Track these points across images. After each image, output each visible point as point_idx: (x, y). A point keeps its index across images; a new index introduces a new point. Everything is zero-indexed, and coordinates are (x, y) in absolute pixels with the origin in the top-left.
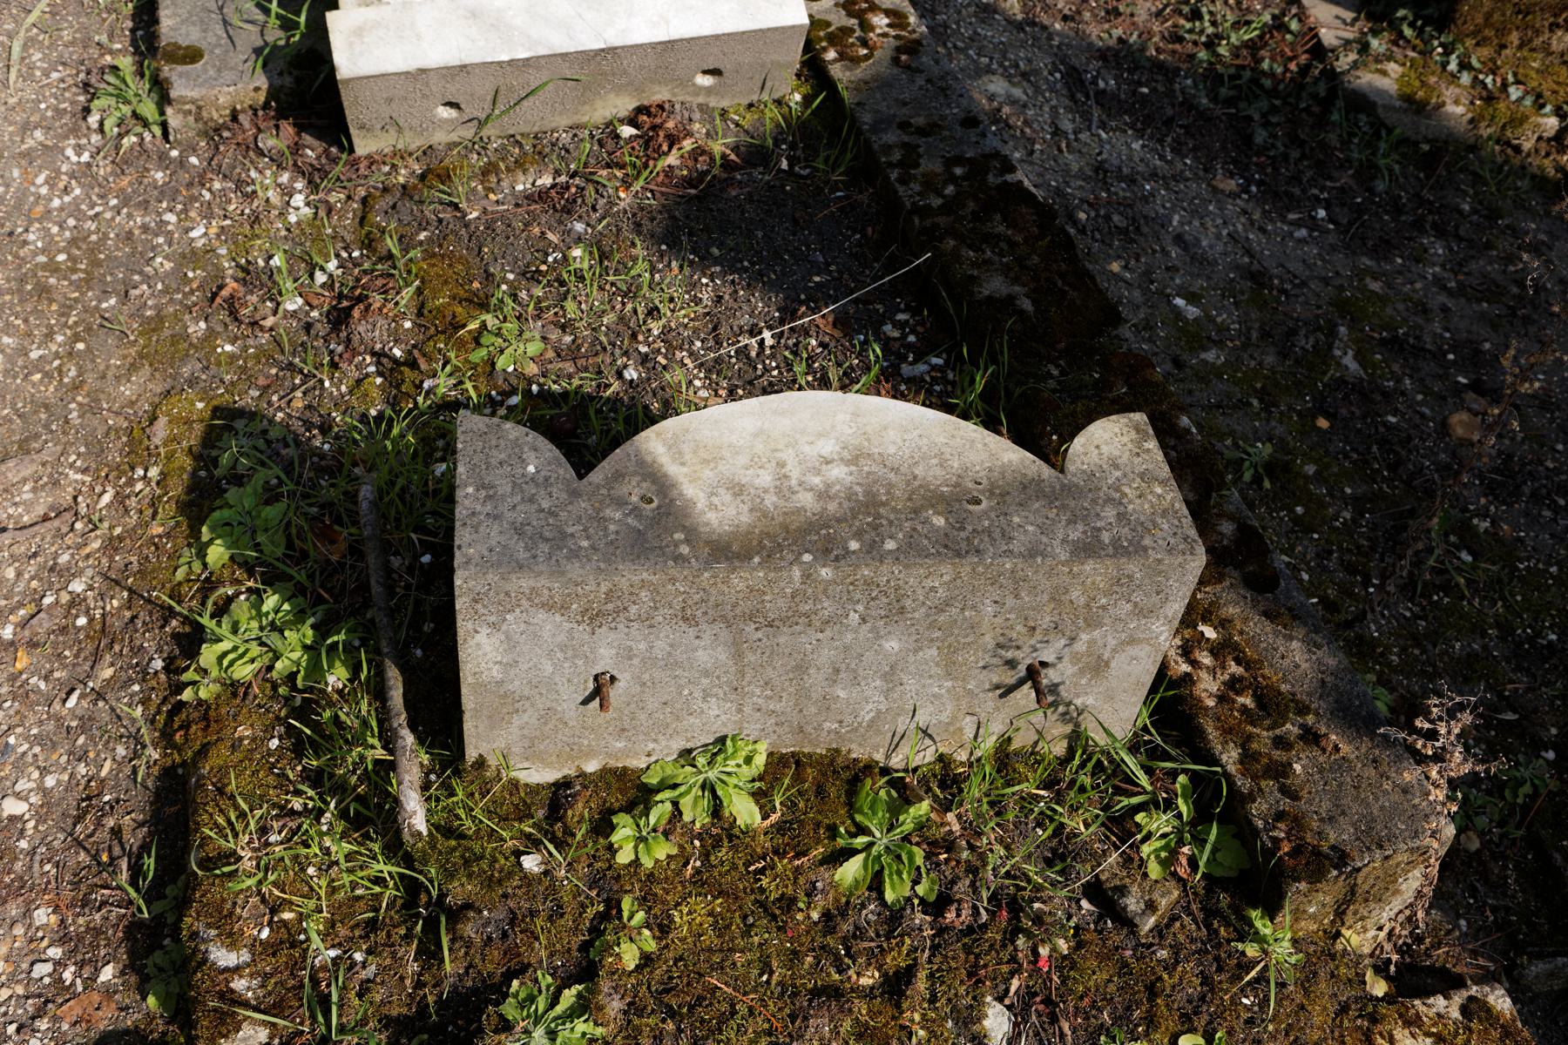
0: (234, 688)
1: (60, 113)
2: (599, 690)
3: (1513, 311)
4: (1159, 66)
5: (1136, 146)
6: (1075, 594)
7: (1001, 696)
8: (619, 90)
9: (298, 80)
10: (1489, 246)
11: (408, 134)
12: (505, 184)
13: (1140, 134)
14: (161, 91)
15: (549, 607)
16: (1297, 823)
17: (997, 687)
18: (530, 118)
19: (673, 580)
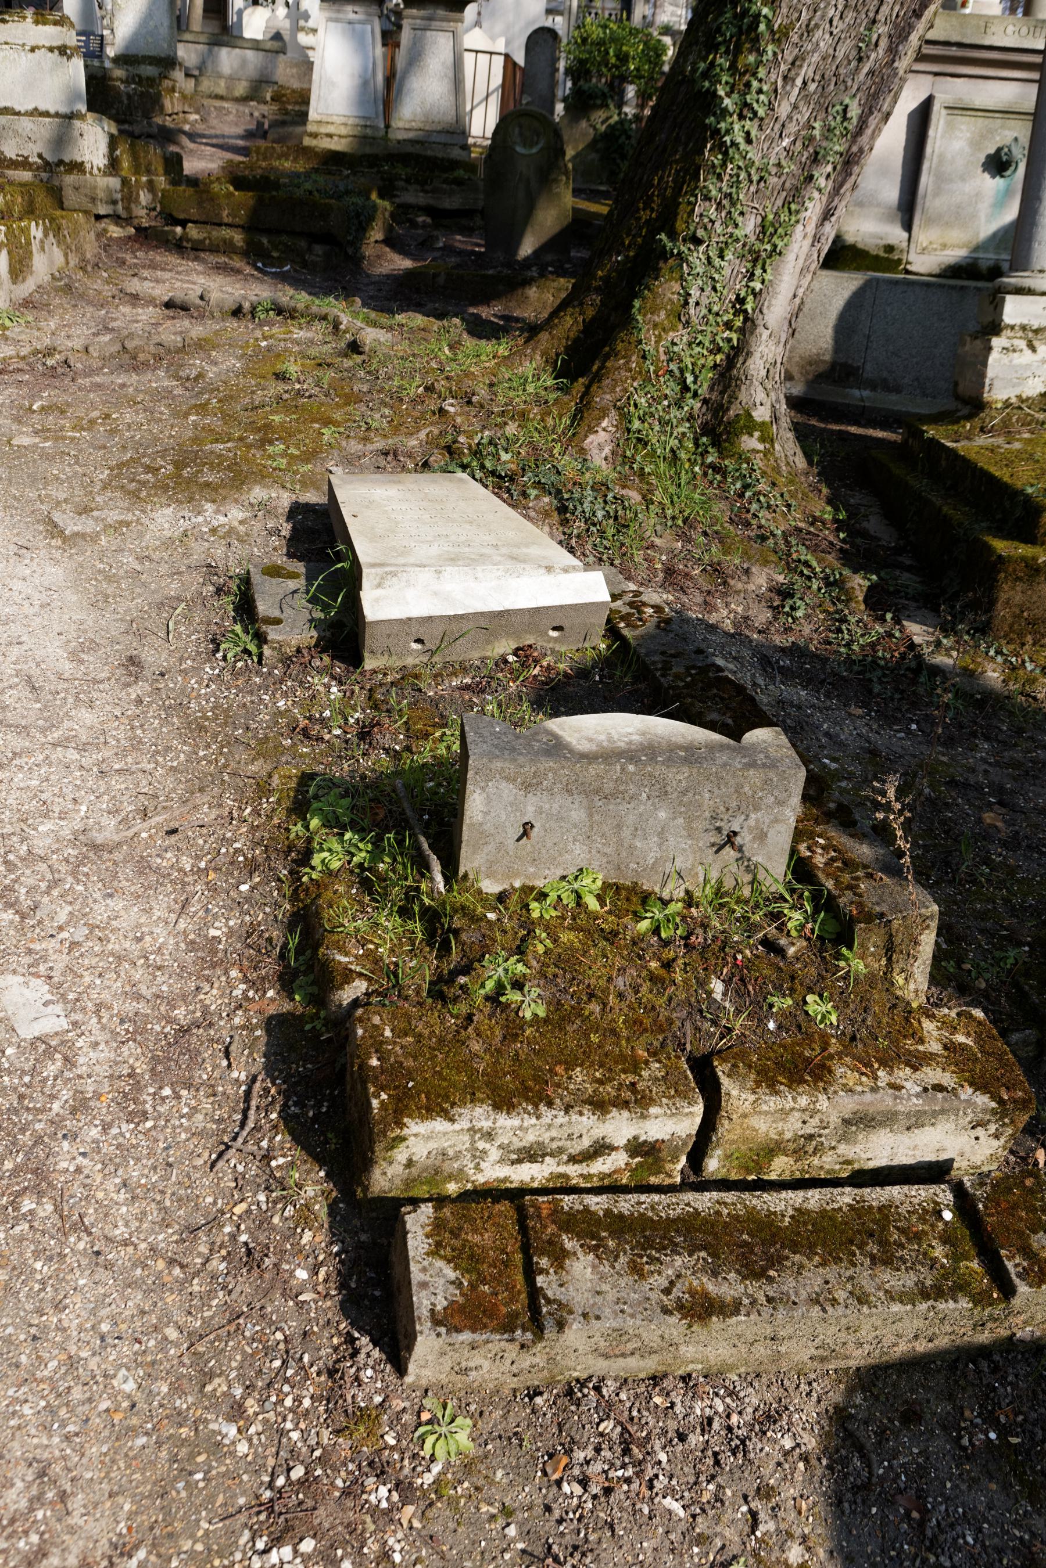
0: (330, 873)
1: (199, 653)
2: (527, 829)
3: (1027, 773)
4: (814, 655)
5: (803, 693)
6: (746, 789)
7: (717, 852)
8: (508, 635)
9: (333, 634)
10: (1016, 745)
11: (394, 657)
12: (446, 682)
13: (804, 688)
14: (261, 638)
15: (507, 779)
16: (860, 905)
17: (713, 845)
18: (458, 653)
19: (563, 767)
